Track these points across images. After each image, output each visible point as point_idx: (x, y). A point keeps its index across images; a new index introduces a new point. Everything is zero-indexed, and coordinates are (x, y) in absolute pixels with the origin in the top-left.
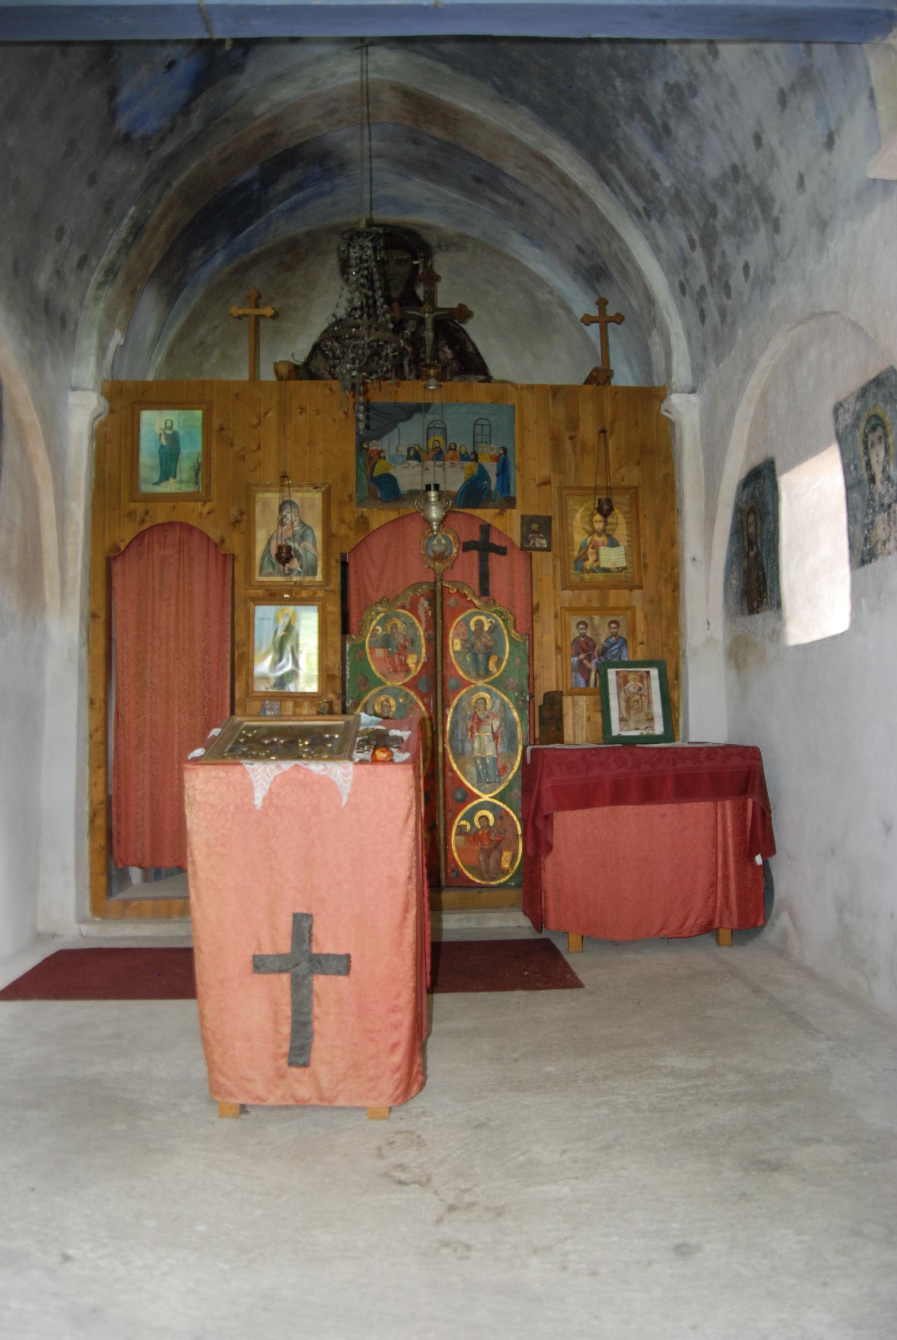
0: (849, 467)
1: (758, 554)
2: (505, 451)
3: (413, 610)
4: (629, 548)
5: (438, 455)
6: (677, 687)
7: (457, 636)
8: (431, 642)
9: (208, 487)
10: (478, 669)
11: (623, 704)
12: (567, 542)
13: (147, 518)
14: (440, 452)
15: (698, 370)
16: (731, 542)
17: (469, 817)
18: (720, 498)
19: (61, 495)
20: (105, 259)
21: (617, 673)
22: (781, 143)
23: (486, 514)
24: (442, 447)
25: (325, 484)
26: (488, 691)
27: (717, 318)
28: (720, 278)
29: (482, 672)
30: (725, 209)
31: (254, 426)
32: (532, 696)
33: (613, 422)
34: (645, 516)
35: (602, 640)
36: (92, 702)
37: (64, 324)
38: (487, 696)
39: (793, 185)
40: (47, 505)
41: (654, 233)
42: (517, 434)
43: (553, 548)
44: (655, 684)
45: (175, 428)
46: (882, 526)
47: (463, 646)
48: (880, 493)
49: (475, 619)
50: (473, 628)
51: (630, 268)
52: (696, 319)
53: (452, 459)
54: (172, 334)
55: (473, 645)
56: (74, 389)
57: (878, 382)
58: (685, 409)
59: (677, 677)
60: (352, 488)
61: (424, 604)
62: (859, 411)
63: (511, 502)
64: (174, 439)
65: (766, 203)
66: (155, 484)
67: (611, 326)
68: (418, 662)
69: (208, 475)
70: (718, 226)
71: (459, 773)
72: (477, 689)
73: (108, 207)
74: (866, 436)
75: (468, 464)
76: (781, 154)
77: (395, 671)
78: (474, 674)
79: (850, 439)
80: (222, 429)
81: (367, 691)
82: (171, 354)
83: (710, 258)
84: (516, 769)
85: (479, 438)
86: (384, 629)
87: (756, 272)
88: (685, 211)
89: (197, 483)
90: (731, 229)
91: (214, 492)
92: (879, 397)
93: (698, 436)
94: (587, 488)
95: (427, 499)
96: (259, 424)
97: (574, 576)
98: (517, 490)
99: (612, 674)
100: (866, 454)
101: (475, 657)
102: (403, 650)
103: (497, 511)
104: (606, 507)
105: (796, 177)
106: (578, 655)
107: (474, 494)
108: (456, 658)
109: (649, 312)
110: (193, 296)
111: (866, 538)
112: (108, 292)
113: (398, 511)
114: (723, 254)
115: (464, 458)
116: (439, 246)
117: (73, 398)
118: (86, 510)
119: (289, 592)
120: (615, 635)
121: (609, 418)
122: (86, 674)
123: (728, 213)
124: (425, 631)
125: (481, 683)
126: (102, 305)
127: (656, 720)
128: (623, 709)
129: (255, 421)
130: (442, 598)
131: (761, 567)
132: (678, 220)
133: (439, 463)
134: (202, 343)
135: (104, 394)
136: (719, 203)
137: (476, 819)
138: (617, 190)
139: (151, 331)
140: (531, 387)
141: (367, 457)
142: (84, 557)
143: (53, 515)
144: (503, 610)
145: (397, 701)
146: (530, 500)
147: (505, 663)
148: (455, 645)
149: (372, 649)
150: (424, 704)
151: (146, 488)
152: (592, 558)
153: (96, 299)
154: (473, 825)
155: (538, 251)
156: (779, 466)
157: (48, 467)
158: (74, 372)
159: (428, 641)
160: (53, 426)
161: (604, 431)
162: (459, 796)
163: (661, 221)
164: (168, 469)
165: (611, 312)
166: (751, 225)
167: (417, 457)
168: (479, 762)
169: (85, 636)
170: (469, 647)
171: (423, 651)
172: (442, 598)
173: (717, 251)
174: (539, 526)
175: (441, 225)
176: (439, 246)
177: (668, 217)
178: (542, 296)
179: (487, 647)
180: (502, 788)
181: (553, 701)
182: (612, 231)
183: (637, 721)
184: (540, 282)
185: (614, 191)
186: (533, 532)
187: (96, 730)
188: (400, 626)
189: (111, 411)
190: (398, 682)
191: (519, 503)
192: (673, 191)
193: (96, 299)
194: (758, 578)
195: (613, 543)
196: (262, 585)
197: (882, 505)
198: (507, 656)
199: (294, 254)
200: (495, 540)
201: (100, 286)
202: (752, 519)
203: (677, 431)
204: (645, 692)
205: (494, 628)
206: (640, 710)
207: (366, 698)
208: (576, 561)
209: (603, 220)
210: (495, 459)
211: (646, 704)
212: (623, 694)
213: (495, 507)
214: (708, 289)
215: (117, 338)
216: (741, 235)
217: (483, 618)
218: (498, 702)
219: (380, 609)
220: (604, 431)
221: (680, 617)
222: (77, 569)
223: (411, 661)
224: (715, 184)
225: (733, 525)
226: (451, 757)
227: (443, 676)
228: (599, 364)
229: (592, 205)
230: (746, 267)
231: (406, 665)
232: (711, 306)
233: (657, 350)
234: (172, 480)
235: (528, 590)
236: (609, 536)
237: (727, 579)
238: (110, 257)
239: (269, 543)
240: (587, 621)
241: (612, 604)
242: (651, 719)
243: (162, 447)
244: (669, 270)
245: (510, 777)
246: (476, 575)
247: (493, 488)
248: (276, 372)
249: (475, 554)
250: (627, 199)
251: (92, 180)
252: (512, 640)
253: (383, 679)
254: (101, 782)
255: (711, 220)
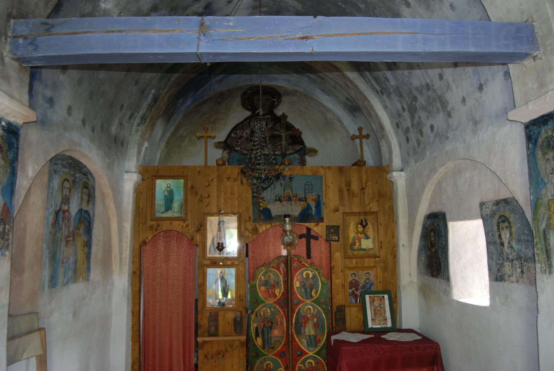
0: (489, 234)
1: (436, 252)
2: (319, 196)
3: (278, 268)
4: (374, 239)
5: (289, 199)
6: (396, 302)
7: (297, 280)
8: (286, 282)
9: (186, 214)
10: (307, 295)
11: (373, 312)
12: (346, 237)
13: (158, 228)
14: (290, 197)
15: (405, 162)
16: (421, 240)
17: (303, 363)
18: (417, 221)
19: (120, 221)
20: (141, 113)
21: (370, 297)
22: (453, 81)
23: (311, 225)
24: (291, 195)
25: (238, 213)
26: (312, 305)
27: (415, 143)
28: (418, 127)
29: (309, 297)
30: (421, 100)
31: (207, 187)
32: (331, 307)
33: (366, 183)
34: (381, 224)
35: (363, 281)
36: (133, 312)
37: (122, 144)
38: (311, 307)
39: (459, 100)
40: (114, 226)
41: (384, 101)
42: (324, 189)
43: (340, 240)
44: (387, 302)
45: (171, 187)
46: (508, 268)
47: (300, 284)
48: (507, 252)
49: (305, 272)
50: (305, 277)
51: (372, 113)
52: (404, 140)
53: (295, 200)
54: (168, 134)
55: (305, 284)
56: (127, 172)
57: (506, 201)
58: (399, 179)
59: (396, 297)
60: (251, 214)
61: (282, 266)
62: (495, 211)
63: (321, 220)
64: (171, 192)
65: (444, 104)
66: (162, 213)
67: (364, 140)
68: (280, 292)
69: (186, 209)
70: (418, 106)
71: (299, 342)
72: (307, 304)
73: (143, 92)
74: (499, 223)
75: (302, 203)
76: (453, 86)
77: (270, 296)
78: (304, 295)
79: (489, 221)
80: (192, 188)
81: (258, 306)
82: (168, 143)
83: (413, 118)
84: (324, 340)
85: (307, 191)
86: (265, 277)
87: (437, 131)
88: (400, 95)
89: (181, 213)
90: (424, 108)
91: (189, 217)
92: (507, 209)
93: (405, 190)
94: (355, 213)
95: (285, 221)
96: (209, 185)
97: (350, 252)
98: (325, 213)
99: (367, 297)
100: (499, 231)
101: (306, 289)
102: (273, 287)
103: (315, 224)
104: (364, 224)
105: (461, 97)
106: (352, 288)
107: (305, 216)
108: (297, 291)
109: (381, 133)
110: (178, 118)
111: (498, 270)
112: (142, 127)
113: (271, 224)
114: (420, 117)
115: (300, 200)
116: (284, 94)
117: (126, 176)
118: (131, 226)
119: (222, 262)
120: (368, 279)
121: (364, 181)
122: (131, 300)
123: (423, 101)
124: (283, 278)
125: (308, 301)
126: (139, 134)
127: (388, 320)
128: (373, 315)
129: (207, 184)
130: (291, 263)
131: (438, 258)
132: (397, 98)
133: (289, 202)
134: (181, 136)
135: (140, 173)
136: (418, 96)
137: (306, 363)
138: (368, 81)
139: (159, 134)
140: (329, 168)
141: (256, 199)
142: (130, 247)
143: (117, 231)
144: (318, 268)
145: (270, 310)
146: (330, 218)
147: (319, 292)
148: (297, 284)
149: (259, 287)
150: (283, 311)
151: (158, 215)
152: (357, 244)
153: (137, 131)
154: (305, 366)
155: (328, 97)
156: (448, 217)
157: (115, 210)
158: (127, 164)
159: (284, 282)
160: (117, 190)
161: (363, 189)
162: (299, 353)
163: (389, 96)
164: (168, 208)
165: (364, 133)
166: (435, 110)
167: (280, 200)
168: (308, 338)
169: (130, 282)
170: (303, 285)
171: (282, 287)
172: (291, 263)
173: (416, 115)
174: (333, 230)
175: (286, 86)
176: (284, 94)
177: (392, 96)
178: (329, 116)
179: (311, 285)
180: (318, 349)
181: (341, 309)
182: (365, 97)
183: (379, 321)
184: (329, 110)
185: (366, 81)
186: (331, 233)
187: (135, 325)
188: (272, 276)
189: (143, 180)
190: (271, 301)
191: (325, 220)
192: (395, 87)
193: (137, 131)
194: (436, 263)
195: (367, 238)
196: (210, 259)
197: (508, 258)
198: (320, 289)
199: (221, 98)
200: (312, 233)
201: (138, 125)
202: (432, 234)
203: (395, 187)
204: (382, 306)
205: (314, 276)
206: (381, 315)
207: (257, 309)
208: (351, 245)
209: (361, 93)
210: (314, 200)
211: (383, 312)
212: (372, 307)
213: (314, 222)
214: (411, 129)
215: (146, 145)
216: (429, 112)
217: (309, 272)
218: (316, 310)
219: (263, 268)
220: (363, 189)
221: (397, 270)
222: (127, 253)
223: (277, 292)
224: (417, 89)
225: (422, 233)
226: (295, 335)
227: (291, 299)
228: (360, 158)
229: (356, 86)
230: (432, 127)
231: (275, 294)
232: (413, 136)
233: (384, 149)
234: (170, 211)
235: (329, 255)
236: (365, 234)
237: (419, 256)
238: (143, 112)
239: (213, 239)
240: (356, 273)
241: (366, 265)
242: (386, 320)
243: (166, 196)
244: (391, 116)
245: (322, 344)
246: (305, 249)
247: (313, 213)
248: (217, 163)
249: (304, 240)
250: (372, 85)
251: (136, 83)
252: (322, 282)
253: (264, 300)
254: (137, 349)
255: (414, 102)
